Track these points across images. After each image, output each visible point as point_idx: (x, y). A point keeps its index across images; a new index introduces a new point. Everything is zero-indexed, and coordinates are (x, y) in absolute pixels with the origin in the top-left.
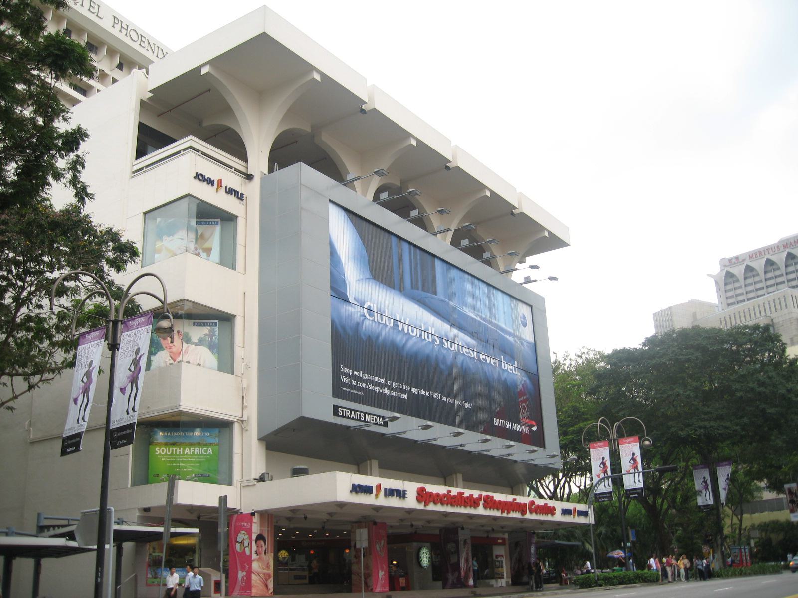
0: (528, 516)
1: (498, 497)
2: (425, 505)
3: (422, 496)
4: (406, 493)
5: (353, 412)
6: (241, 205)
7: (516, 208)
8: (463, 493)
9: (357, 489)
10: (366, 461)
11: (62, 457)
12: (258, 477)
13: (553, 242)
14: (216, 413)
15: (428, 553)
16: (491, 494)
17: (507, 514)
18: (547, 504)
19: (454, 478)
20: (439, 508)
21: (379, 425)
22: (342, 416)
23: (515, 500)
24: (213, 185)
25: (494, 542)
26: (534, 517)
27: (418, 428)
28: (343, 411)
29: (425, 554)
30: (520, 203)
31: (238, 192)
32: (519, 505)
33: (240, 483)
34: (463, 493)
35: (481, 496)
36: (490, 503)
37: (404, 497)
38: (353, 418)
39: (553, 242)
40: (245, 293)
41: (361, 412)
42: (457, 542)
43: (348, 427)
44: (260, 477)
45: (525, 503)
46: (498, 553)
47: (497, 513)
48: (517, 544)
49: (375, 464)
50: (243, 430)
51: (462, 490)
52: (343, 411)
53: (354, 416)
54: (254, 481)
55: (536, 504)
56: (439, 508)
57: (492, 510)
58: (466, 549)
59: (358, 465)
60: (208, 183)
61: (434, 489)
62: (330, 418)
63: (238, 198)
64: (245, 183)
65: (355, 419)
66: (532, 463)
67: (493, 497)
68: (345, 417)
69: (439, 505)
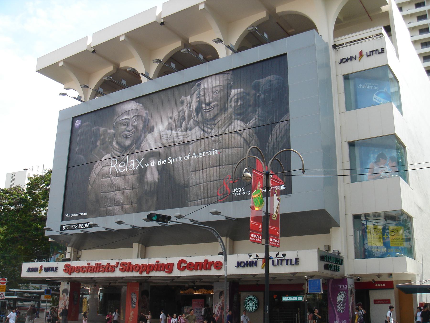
0: (176, 272)
3: (69, 269)
15: (256, 300)
16: (127, 261)
26: (187, 273)
29: (251, 301)
58: (222, 299)
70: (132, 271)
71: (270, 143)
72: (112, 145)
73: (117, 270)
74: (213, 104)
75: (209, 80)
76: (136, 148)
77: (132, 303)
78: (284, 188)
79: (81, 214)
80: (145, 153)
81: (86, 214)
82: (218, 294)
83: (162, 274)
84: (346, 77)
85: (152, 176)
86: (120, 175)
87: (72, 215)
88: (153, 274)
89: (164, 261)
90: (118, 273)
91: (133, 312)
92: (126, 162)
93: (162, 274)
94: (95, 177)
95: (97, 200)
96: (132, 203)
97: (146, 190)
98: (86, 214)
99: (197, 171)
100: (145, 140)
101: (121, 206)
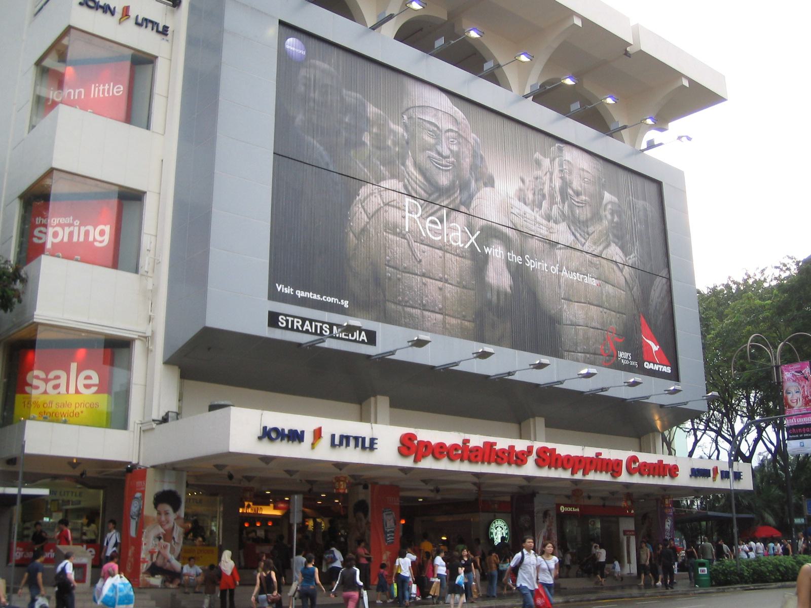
0: (624, 478)
1: (563, 450)
2: (416, 460)
3: (407, 445)
4: (376, 441)
5: (307, 323)
6: (164, 42)
7: (629, 45)
8: (495, 444)
9: (268, 434)
10: (528, 418)
11: (320, 426)
12: (160, 418)
13: (699, 97)
14: (86, 325)
15: (505, 527)
16: (550, 445)
17: (584, 474)
18: (662, 461)
19: (651, 439)
20: (444, 465)
21: (359, 342)
22: (286, 328)
23: (600, 454)
24: (113, 13)
25: (622, 513)
26: (636, 479)
27: (529, 367)
28: (287, 321)
29: (499, 529)
30: (636, 36)
31: (157, 24)
32: (608, 462)
33: (140, 425)
34: (495, 444)
35: (530, 449)
36: (546, 458)
37: (372, 448)
38: (307, 332)
39: (699, 97)
40: (162, 161)
41: (324, 323)
42: (532, 514)
43: (299, 345)
44: (163, 417)
45: (620, 458)
46: (626, 528)
47: (566, 474)
48: (645, 516)
49: (540, 422)
50: (148, 351)
51: (467, 436)
52: (287, 321)
53: (309, 328)
54: (153, 423)
55: (641, 461)
56: (444, 465)
57: (651, 476)
58: (547, 524)
59: (639, 437)
60: (105, 12)
61: (425, 435)
62: (262, 330)
63: (158, 31)
64: (173, 12)
65: (311, 333)
66: (510, 377)
67: (554, 450)
68: (292, 329)
69: (445, 460)
70: (489, 463)
71: (652, 301)
72: (404, 164)
73: (531, 460)
74: (583, 198)
75: (576, 153)
76: (462, 203)
77: (386, 533)
78: (670, 371)
79: (330, 300)
80: (482, 223)
81: (346, 303)
82: (541, 515)
83: (605, 477)
84: (142, 61)
85: (498, 277)
86: (432, 245)
87: (300, 294)
88: (592, 476)
89: (609, 454)
90: (530, 469)
91: (388, 553)
92: (442, 221)
93: (605, 477)
94: (366, 219)
95: (378, 280)
96: (464, 318)
97: (490, 302)
98: (346, 303)
99: (571, 301)
100: (478, 195)
101: (440, 317)
